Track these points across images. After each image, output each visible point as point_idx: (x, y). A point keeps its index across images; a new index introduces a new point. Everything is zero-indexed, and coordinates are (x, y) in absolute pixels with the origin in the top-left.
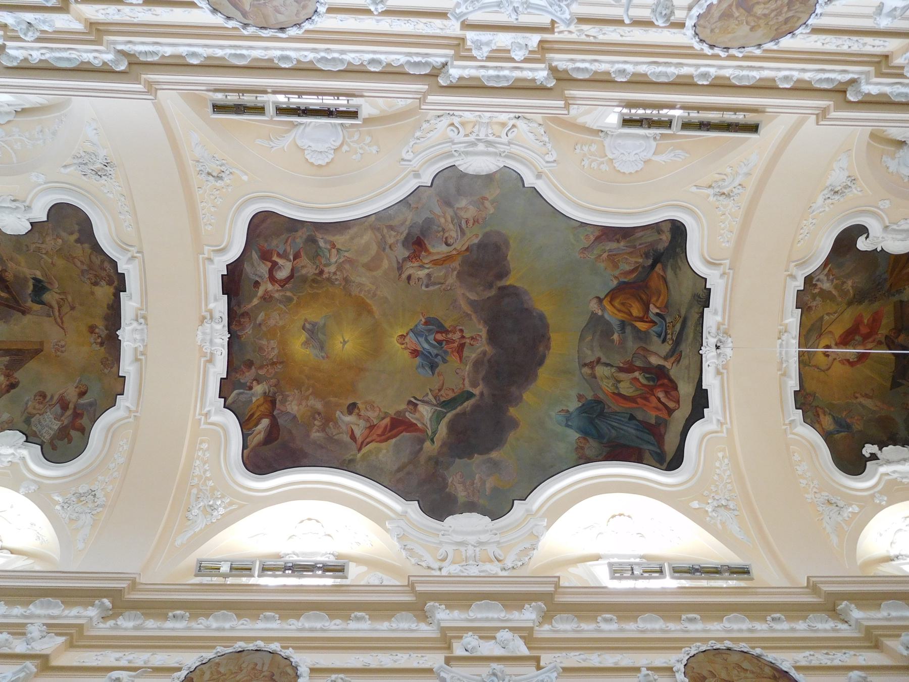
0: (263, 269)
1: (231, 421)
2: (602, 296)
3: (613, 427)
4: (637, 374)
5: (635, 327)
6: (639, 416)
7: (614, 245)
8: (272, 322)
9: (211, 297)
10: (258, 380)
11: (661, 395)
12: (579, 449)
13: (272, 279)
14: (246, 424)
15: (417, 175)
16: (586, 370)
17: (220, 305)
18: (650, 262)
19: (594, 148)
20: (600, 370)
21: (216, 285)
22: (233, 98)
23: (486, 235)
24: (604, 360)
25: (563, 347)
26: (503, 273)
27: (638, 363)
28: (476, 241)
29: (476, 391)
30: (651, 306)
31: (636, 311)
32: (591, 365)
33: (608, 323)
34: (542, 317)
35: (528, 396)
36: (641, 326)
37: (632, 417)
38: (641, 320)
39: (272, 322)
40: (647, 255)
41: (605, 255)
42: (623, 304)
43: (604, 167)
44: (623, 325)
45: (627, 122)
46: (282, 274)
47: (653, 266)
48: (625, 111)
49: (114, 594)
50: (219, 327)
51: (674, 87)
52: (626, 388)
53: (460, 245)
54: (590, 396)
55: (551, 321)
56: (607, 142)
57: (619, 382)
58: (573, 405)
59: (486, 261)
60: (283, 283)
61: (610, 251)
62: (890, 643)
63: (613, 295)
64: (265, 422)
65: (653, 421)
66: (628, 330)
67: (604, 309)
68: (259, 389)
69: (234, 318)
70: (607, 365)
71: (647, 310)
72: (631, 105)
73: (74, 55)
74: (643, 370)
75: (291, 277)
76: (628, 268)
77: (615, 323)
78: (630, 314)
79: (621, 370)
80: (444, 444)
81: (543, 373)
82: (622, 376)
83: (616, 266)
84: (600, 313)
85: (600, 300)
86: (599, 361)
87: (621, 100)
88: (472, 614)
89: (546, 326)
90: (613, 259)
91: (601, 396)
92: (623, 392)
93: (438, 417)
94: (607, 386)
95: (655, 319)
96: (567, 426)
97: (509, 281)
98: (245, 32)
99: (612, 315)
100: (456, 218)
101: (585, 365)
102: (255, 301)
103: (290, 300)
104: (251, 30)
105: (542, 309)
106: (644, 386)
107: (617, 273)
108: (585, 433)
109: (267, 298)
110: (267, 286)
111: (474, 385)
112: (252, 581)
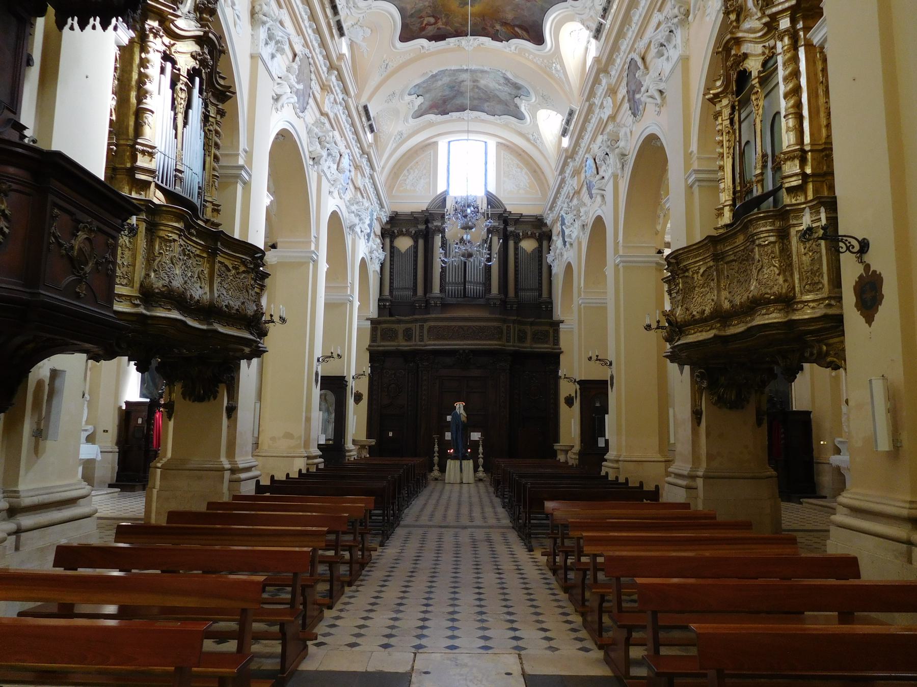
0: (430, 28)
9: (447, 47)
10: (493, 27)
13: (435, 23)
17: (452, 41)
21: (441, 44)
45: (342, 34)
46: (432, 20)
49: (566, 158)
50: (463, 42)
60: (437, 19)
64: (516, 29)
68: (498, 27)
73: (302, 10)
75: (433, 16)
102: (448, 28)
103: (446, 15)
104: (312, 62)
110: (440, 24)
112: (608, 26)
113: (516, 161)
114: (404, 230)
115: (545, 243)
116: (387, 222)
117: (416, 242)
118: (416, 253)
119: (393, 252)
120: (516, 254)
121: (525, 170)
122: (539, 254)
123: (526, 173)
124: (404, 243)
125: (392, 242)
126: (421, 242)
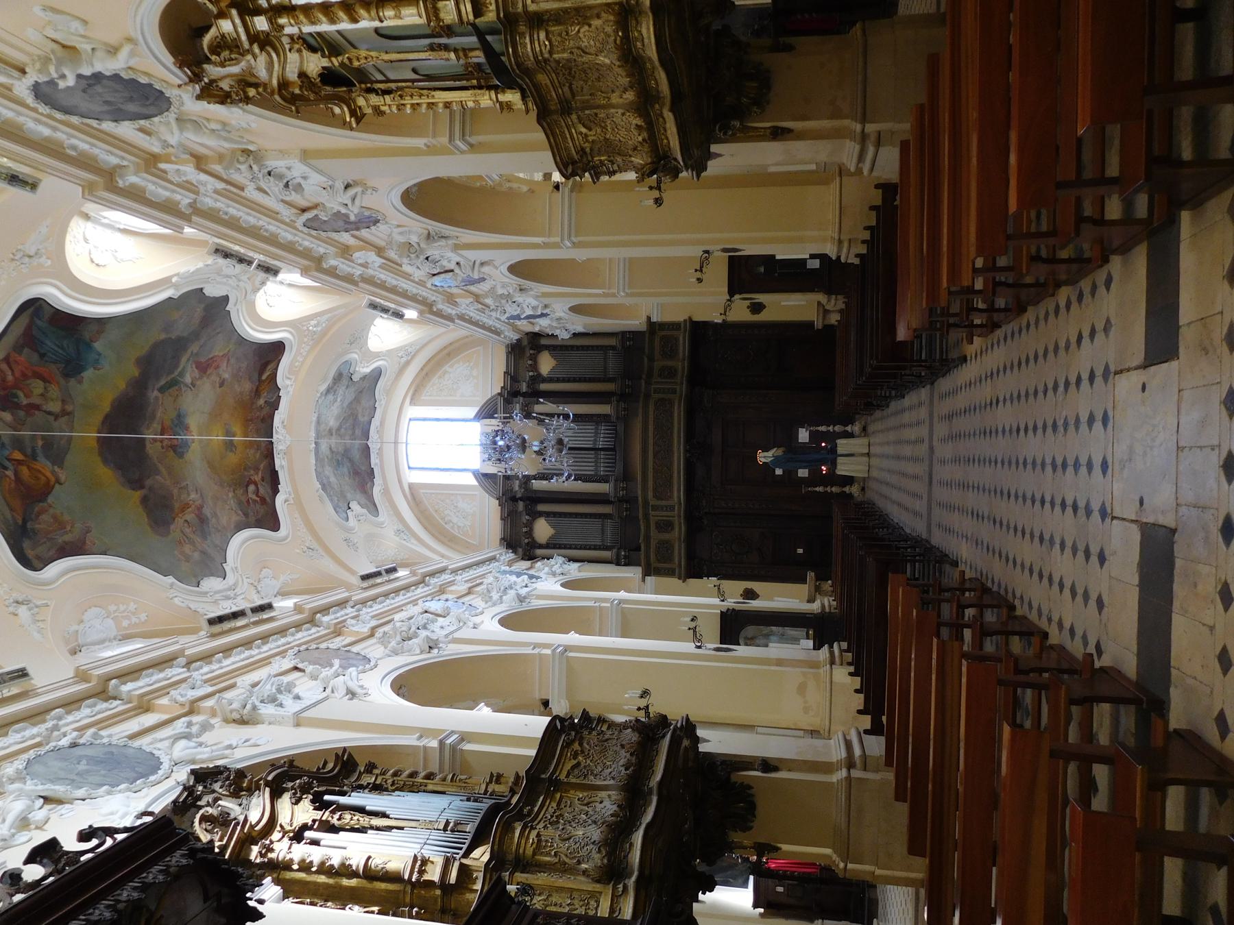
0: (262, 491)
1: (280, 381)
2: (57, 486)
3: (62, 348)
4: (25, 402)
5: (25, 454)
6: (35, 357)
7: (67, 538)
8: (252, 451)
10: (261, 408)
11: (10, 378)
12: (100, 332)
13: (256, 484)
14: (273, 377)
15: (172, 585)
16: (69, 408)
17: (279, 462)
18: (29, 525)
19: (125, 623)
20: (55, 407)
22: (227, 625)
23: (168, 533)
24: (51, 418)
25: (87, 434)
26: (144, 500)
27: (22, 413)
28: (172, 527)
29: (156, 393)
30: (13, 478)
31: (24, 470)
32: (64, 413)
33: (47, 457)
34: (105, 461)
35: (122, 385)
36: (18, 455)
37: (42, 356)
38: (19, 462)
39: (252, 451)
40: (33, 530)
41: (69, 528)
42: (38, 479)
43: (112, 608)
44: (34, 457)
46: (252, 488)
47: (25, 521)
48: (272, 614)
51: (76, 698)
52: (37, 387)
53: (179, 521)
54: (72, 382)
55: (98, 459)
56: (114, 633)
57: (42, 395)
58: (88, 374)
59: (160, 510)
60: (250, 482)
61: (66, 533)
62: (164, 701)
63: (47, 490)
64: (264, 378)
65: (26, 350)
66: (29, 451)
67: (53, 472)
68: (261, 402)
69: (269, 454)
70: (50, 413)
71: (16, 473)
72: (271, 619)
73: (147, 680)
74: (18, 406)
75: (247, 486)
76: (44, 517)
77: (41, 458)
78: (29, 467)
79: (37, 407)
80: (185, 350)
81: (106, 407)
82: (36, 400)
83: (55, 517)
84: (56, 468)
85: (58, 481)
86: (57, 417)
87: (38, 695)
88: (167, 194)
89: (101, 454)
90: (61, 525)
91: (62, 381)
92: (40, 383)
93: (181, 374)
94: (54, 391)
95: (7, 464)
96: (100, 354)
97: (138, 494)
98: (92, 730)
99: (44, 465)
100: (193, 543)
101: (69, 414)
102: (262, 466)
103: (245, 469)
105: (106, 470)
106: (21, 389)
107: (51, 511)
108: (89, 346)
109: (257, 469)
110: (257, 478)
111: (157, 398)
112: (262, 257)
113: (435, 380)
114: (525, 530)
115: (544, 342)
116: (515, 552)
117: (541, 514)
118: (555, 514)
119: (554, 545)
120: (558, 380)
121: (446, 367)
122: (558, 349)
123: (451, 366)
124: (543, 530)
125: (541, 546)
126: (541, 507)
